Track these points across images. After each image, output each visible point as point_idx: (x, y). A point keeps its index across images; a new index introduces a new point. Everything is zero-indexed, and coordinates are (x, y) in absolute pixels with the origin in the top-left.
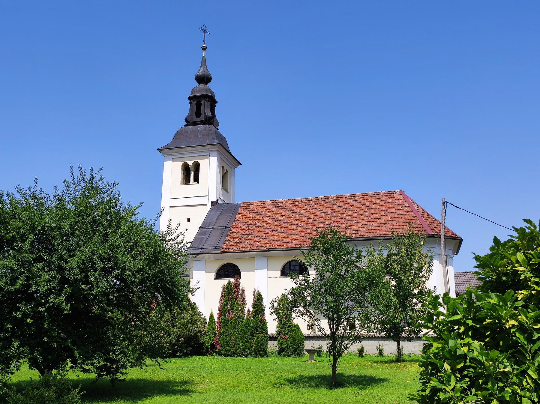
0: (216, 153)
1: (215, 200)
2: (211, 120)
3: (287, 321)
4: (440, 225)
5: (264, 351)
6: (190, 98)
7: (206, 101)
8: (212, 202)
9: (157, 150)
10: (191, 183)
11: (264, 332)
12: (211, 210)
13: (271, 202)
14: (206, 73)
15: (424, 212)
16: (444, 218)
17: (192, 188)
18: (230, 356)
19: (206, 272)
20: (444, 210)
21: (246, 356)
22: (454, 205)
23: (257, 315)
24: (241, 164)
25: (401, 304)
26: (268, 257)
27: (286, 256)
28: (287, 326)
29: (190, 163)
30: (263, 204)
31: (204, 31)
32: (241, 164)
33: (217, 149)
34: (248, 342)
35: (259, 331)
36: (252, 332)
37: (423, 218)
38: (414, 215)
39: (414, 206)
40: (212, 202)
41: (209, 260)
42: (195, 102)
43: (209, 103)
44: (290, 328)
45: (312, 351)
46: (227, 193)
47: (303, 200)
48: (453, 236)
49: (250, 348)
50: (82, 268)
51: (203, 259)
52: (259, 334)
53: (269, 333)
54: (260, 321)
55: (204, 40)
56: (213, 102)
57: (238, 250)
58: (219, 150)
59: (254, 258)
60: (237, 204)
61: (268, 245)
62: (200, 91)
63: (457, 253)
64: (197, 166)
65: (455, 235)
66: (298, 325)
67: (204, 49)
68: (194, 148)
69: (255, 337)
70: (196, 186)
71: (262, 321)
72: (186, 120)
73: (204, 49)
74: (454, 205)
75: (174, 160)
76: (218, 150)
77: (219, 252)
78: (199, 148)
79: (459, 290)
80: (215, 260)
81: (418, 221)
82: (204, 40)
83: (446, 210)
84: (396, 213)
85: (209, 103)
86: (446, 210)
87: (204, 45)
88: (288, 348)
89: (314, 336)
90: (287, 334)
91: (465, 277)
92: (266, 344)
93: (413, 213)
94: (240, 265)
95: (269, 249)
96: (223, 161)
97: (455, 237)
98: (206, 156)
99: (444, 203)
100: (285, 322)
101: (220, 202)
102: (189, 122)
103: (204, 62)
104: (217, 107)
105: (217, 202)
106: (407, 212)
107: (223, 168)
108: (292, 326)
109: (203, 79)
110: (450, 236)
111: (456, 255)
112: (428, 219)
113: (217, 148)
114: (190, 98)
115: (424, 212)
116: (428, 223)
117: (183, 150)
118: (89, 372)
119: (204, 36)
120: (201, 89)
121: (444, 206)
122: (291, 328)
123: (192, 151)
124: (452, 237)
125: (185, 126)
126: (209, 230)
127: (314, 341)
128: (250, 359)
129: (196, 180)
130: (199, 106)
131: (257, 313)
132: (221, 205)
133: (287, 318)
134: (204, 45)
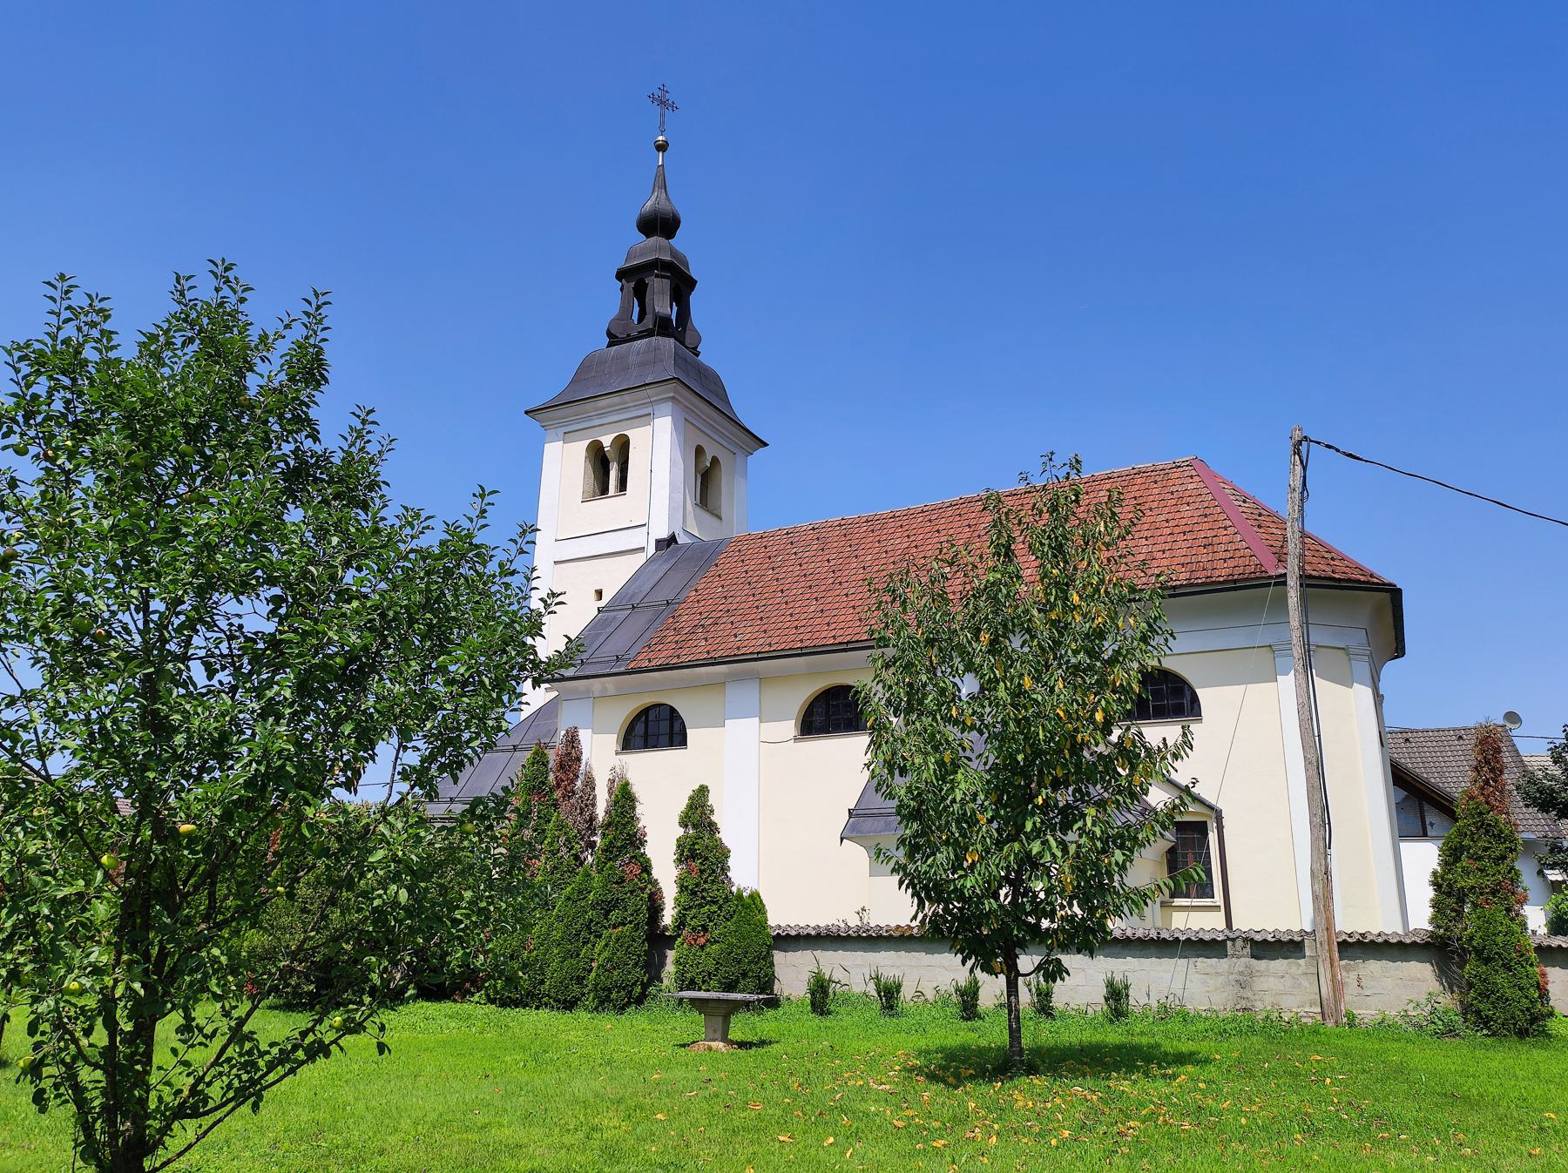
0: (668, 406)
1: (664, 535)
2: (677, 328)
3: (706, 882)
4: (1284, 526)
5: (624, 988)
6: (622, 275)
7: (657, 276)
8: (658, 542)
9: (526, 412)
11: (631, 922)
12: (650, 561)
13: (811, 527)
14: (664, 205)
15: (1265, 513)
16: (1297, 495)
17: (611, 509)
18: (517, 1004)
19: (594, 733)
20: (1299, 469)
21: (569, 1005)
22: (1338, 450)
23: (610, 859)
24: (766, 445)
25: (1005, 807)
26: (762, 679)
27: (812, 673)
28: (703, 898)
29: (607, 441)
30: (787, 533)
31: (663, 103)
32: (766, 445)
33: (671, 395)
34: (578, 955)
35: (613, 916)
36: (591, 921)
37: (1256, 529)
38: (1228, 523)
39: (1232, 497)
40: (658, 542)
43: (667, 282)
44: (714, 908)
45: (714, 1005)
46: (715, 520)
48: (1362, 578)
49: (584, 978)
52: (615, 927)
53: (772, 922)
54: (616, 883)
55: (662, 124)
56: (682, 286)
58: (677, 397)
59: (719, 685)
60: (1195, 699)
61: (760, 644)
62: (643, 252)
63: (1399, 651)
64: (623, 445)
65: (1372, 576)
66: (755, 896)
67: (661, 148)
68: (615, 399)
69: (600, 936)
71: (623, 881)
72: (609, 334)
73: (661, 148)
74: (1338, 450)
75: (568, 437)
76: (673, 398)
77: (622, 669)
78: (627, 397)
79: (1444, 780)
81: (1239, 537)
82: (662, 124)
83: (1305, 468)
84: (1167, 521)
85: (667, 282)
86: (1305, 468)
87: (660, 138)
88: (704, 982)
89: (819, 934)
90: (705, 928)
91: (1462, 742)
92: (632, 963)
93: (1224, 516)
95: (758, 653)
96: (697, 427)
97: (1368, 582)
98: (646, 418)
99: (1300, 442)
100: (697, 885)
101: (682, 539)
102: (617, 337)
103: (661, 183)
104: (696, 299)
105: (672, 539)
106: (1206, 516)
107: (699, 451)
108: (727, 900)
109: (660, 224)
110: (1349, 580)
111: (1397, 657)
112: (1275, 531)
113: (669, 390)
114: (622, 275)
115: (1265, 513)
116: (1271, 543)
117: (589, 406)
119: (662, 115)
120: (652, 248)
121: (1297, 452)
122: (720, 908)
123: (610, 407)
124: (1359, 581)
126: (623, 615)
127: (818, 953)
128: (582, 1016)
129: (622, 485)
130: (640, 292)
131: (611, 852)
132: (688, 547)
133: (704, 870)
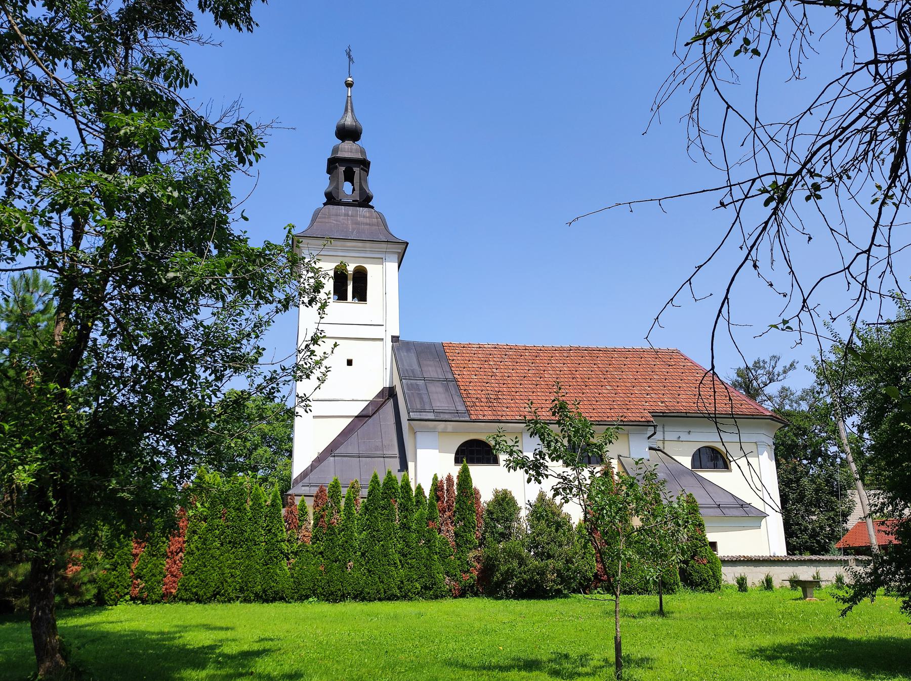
7: (362, 169)
8: (393, 337)
10: (349, 301)
41: (444, 432)
42: (343, 168)
47: (520, 348)
50: (600, 447)
51: (433, 430)
57: (499, 418)
64: (361, 277)
67: (349, 85)
68: (360, 244)
70: (359, 307)
78: (368, 245)
80: (455, 432)
87: (350, 79)
94: (733, 450)
98: (380, 260)
117: (339, 243)
118: (522, 664)
125: (325, 204)
134: (350, 79)
